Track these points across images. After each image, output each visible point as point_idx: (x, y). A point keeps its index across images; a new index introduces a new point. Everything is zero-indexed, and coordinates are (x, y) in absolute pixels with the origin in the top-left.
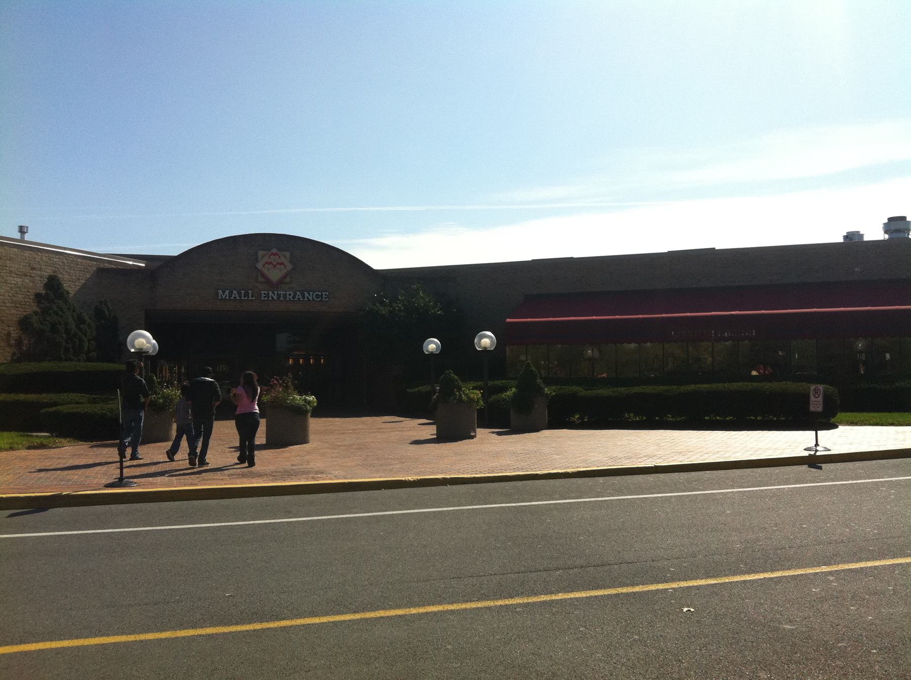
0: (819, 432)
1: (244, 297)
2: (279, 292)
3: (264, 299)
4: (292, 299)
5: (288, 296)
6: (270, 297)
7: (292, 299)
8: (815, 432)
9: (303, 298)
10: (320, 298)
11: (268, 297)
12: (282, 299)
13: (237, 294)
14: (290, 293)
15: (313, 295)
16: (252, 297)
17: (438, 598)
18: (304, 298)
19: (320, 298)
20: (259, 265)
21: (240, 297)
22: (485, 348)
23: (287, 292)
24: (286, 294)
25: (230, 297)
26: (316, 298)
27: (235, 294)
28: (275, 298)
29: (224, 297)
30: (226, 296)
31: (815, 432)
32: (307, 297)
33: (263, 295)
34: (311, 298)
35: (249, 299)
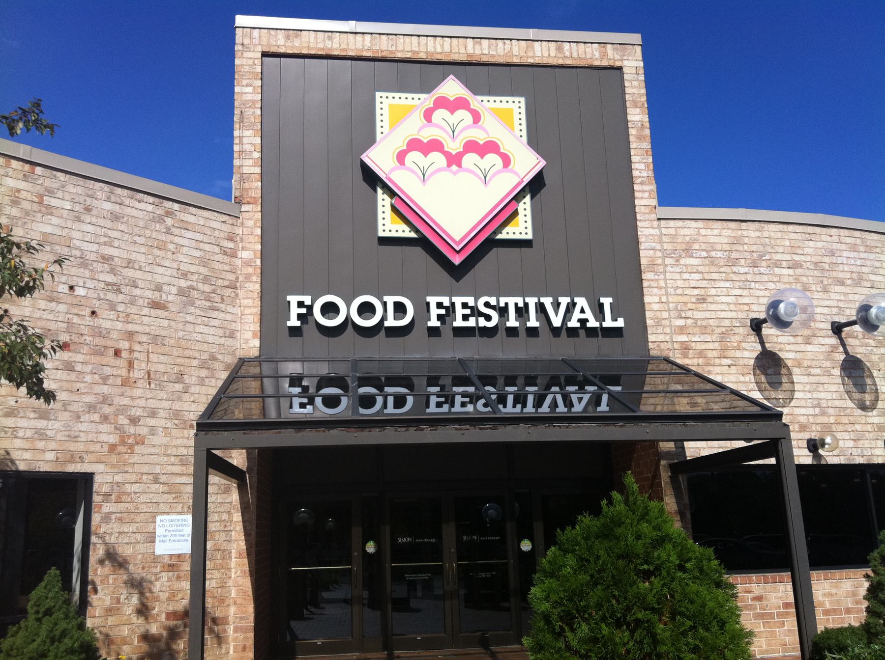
0: (236, 25)
27: (582, 311)
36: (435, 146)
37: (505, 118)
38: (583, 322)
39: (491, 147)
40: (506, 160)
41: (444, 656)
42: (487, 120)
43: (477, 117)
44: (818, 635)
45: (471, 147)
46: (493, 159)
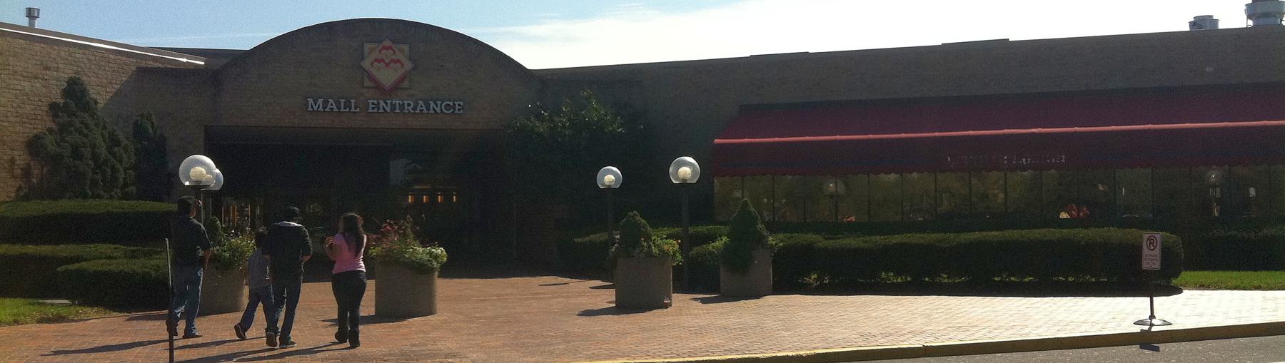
0: (1154, 298)
7: (412, 111)
10: (452, 110)
18: (428, 109)
19: (452, 110)
20: (366, 64)
25: (324, 108)
27: (332, 105)
28: (388, 109)
29: (315, 108)
33: (371, 106)
36: (382, 60)
37: (402, 51)
38: (421, 111)
39: (398, 61)
40: (402, 65)
41: (172, 288)
42: (397, 52)
43: (394, 52)
44: (731, 241)
45: (392, 61)
46: (399, 65)
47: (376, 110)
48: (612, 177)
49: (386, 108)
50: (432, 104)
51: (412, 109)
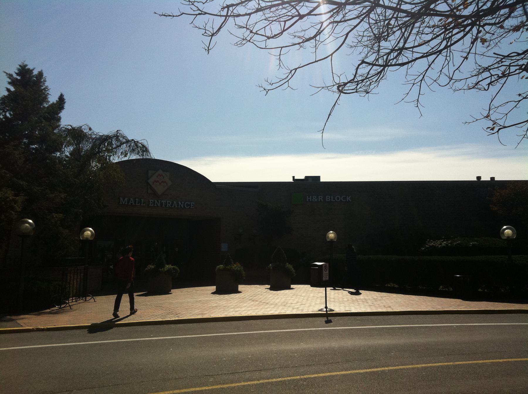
0: (327, 288)
1: (143, 204)
2: (162, 201)
3: (192, 208)
4: (170, 206)
5: (168, 204)
6: (156, 204)
7: (170, 206)
8: (325, 288)
9: (135, 203)
10: (189, 207)
11: (154, 204)
12: (163, 206)
13: (133, 201)
14: (170, 202)
15: (184, 204)
16: (143, 204)
17: (178, 383)
18: (178, 206)
19: (189, 207)
20: (150, 181)
21: (135, 203)
22: (87, 238)
23: (191, 203)
24: (167, 202)
25: (128, 202)
26: (187, 206)
27: (132, 201)
28: (159, 205)
29: (124, 203)
30: (125, 202)
31: (325, 288)
32: (158, 203)
33: (151, 203)
34: (182, 206)
35: (141, 205)
40: (167, 184)
47: (153, 205)
48: (89, 232)
49: (182, 206)
50: (180, 203)
51: (333, 200)
